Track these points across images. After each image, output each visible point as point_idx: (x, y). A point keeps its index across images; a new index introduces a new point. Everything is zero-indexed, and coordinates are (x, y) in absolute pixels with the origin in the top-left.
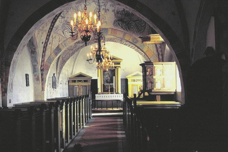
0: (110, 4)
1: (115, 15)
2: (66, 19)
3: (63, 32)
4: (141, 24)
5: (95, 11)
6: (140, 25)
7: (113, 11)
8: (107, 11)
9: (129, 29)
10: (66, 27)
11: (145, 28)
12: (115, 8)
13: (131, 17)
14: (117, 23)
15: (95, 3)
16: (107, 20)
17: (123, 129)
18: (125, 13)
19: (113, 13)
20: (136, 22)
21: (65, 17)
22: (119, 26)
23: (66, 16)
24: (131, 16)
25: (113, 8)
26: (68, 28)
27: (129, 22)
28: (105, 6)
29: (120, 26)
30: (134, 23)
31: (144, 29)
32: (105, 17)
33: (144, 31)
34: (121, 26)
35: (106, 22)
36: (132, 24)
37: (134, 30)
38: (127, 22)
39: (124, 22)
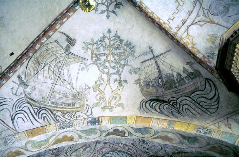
1: (142, 90)
2: (28, 90)
3: (12, 117)
4: (206, 96)
5: (96, 82)
6: (203, 99)
7: (137, 82)
9: (179, 112)
10: (26, 109)
11: (219, 98)
12: (140, 75)
13: (179, 88)
14: (147, 105)
15: (98, 67)
16: (123, 101)
17: (95, 130)
18: (163, 82)
19: (137, 87)
20: (193, 95)
21: (27, 86)
22: (154, 111)
23: (31, 84)
24: (177, 85)
25: (136, 77)
26: (28, 112)
27: (176, 99)
28: (120, 75)
29: (156, 110)
31: (216, 103)
32: (120, 95)
33: (218, 107)
34: (158, 110)
35: (121, 105)
37: (194, 112)
39: (165, 102)
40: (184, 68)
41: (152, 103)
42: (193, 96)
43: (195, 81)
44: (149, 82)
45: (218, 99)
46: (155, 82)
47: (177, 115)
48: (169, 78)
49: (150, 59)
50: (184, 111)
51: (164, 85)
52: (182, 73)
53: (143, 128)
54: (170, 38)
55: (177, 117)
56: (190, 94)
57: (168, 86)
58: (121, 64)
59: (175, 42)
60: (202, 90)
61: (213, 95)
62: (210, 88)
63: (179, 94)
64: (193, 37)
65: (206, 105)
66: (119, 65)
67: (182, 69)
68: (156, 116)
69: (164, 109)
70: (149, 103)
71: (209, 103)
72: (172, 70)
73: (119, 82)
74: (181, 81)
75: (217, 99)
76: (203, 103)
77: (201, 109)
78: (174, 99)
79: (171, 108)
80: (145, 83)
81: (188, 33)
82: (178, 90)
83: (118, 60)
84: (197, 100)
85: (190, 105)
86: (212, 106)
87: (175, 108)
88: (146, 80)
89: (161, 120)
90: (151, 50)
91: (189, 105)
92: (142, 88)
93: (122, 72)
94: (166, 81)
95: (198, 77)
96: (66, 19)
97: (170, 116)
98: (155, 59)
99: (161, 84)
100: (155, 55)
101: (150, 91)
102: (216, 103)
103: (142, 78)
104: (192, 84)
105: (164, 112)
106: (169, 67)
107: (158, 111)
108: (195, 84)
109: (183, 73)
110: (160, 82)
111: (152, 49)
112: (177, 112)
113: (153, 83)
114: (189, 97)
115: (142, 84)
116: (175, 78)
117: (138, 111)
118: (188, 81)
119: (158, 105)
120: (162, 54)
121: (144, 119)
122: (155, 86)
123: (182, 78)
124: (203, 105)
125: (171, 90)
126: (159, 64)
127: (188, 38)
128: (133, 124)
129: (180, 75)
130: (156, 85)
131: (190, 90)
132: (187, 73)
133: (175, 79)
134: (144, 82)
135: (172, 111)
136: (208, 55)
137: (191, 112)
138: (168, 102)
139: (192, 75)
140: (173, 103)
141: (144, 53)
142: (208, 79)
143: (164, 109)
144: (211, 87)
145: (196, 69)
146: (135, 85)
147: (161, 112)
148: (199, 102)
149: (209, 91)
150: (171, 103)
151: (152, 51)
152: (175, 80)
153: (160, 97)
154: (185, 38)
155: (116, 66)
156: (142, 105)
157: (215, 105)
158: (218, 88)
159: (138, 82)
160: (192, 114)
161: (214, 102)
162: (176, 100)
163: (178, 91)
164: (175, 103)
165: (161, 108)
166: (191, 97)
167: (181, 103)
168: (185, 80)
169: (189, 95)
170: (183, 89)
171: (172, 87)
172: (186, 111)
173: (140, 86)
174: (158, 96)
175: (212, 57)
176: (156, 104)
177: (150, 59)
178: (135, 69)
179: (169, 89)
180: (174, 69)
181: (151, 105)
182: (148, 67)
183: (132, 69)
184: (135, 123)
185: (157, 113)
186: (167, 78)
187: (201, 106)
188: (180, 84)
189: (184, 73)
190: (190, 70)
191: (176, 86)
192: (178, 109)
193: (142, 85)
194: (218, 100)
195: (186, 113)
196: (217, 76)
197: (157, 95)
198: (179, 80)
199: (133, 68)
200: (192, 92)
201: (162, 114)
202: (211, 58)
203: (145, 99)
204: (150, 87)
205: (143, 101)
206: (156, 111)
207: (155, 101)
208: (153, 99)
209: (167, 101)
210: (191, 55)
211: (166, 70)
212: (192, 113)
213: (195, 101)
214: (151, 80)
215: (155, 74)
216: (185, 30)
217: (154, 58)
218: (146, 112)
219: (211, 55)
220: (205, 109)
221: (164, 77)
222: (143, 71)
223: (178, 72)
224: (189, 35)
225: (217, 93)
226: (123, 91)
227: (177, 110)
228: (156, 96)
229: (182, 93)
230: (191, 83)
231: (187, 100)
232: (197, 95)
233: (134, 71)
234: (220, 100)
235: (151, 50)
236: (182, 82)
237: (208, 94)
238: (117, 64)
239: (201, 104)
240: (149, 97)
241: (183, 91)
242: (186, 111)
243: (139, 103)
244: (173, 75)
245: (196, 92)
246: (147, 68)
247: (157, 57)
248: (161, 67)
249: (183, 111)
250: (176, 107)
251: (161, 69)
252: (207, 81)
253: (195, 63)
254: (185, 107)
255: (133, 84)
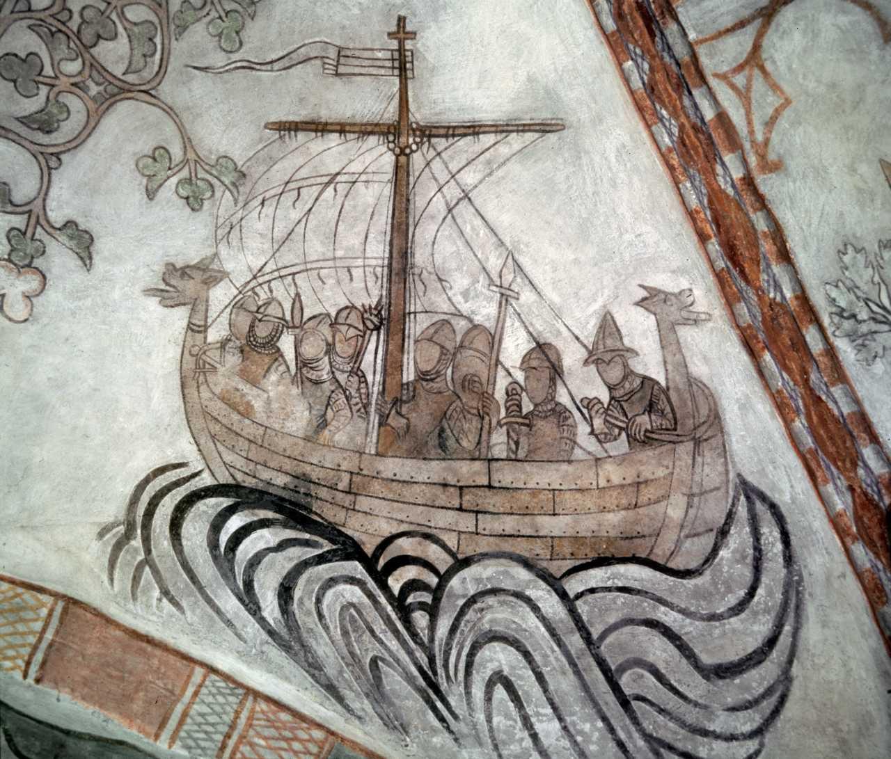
0: (145, 145)
6: (659, 651)
8: (59, 258)
11: (780, 692)
13: (506, 475)
14: (195, 530)
18: (392, 366)
20: (596, 577)
22: (230, 603)
24: (499, 442)
28: (49, 162)
29: (248, 597)
30: (551, 604)
31: (746, 722)
36: (497, 614)
38: (403, 561)
39: (349, 549)
40: (608, 326)
41: (235, 523)
42: (592, 591)
43: (651, 464)
44: (284, 325)
45: (774, 700)
46: (330, 348)
47: (411, 703)
48: (450, 355)
49: (366, 130)
50: (478, 692)
51: (397, 402)
52: (572, 357)
53: (93, 738)
54: (601, 27)
55: (405, 729)
56: (569, 564)
57: (421, 417)
58: (95, 66)
59: (627, 81)
60: (677, 563)
61: (753, 643)
62: (748, 574)
63: (487, 523)
64: (788, 102)
65: (662, 711)
66: (73, 67)
67: (589, 332)
68: (241, 655)
69: (321, 616)
70: (213, 513)
71: (696, 704)
72: (506, 297)
73: (19, 221)
74: (540, 424)
75: (769, 692)
76: (651, 679)
77: (612, 730)
78: (433, 552)
79: (379, 626)
80: (244, 321)
81: (757, 47)
82: (490, 487)
83: (84, 21)
84: (610, 639)
85: (538, 658)
86: (705, 733)
87: (414, 635)
88: (263, 295)
89: (263, 706)
90: (401, 50)
91: (527, 655)
92: (196, 356)
93: (77, 143)
94: (423, 376)
95: (689, 446)
96: (808, 441)
97: (348, 695)
98: (403, 140)
99: (374, 379)
100: (419, 115)
101: (258, 405)
102: (747, 728)
103: (229, 266)
104: (616, 480)
105: (312, 643)
106: (494, 263)
107: (265, 614)
108: (648, 493)
109: (586, 362)
110: (368, 358)
111: (409, 45)
112: (421, 682)
113: (309, 350)
114: (554, 583)
115: (213, 314)
116: (501, 372)
117: (95, 552)
118: (591, 445)
119: (279, 556)
120: (474, 130)
121: (126, 648)
122: (317, 383)
123: (563, 398)
124: (643, 699)
125: (434, 470)
126: (419, 202)
127: (744, 95)
128: (18, 675)
129: (556, 371)
130: (325, 376)
131: (586, 525)
132: (615, 374)
133: (502, 383)
134: (238, 305)
135: (374, 649)
136: (843, 304)
137: (527, 723)
138: (369, 563)
139: (651, 408)
140: (412, 586)
141: (333, 53)
142: (763, 498)
143: (321, 616)
144: (757, 569)
145: (699, 369)
146: (153, 303)
147: (284, 632)
148: (621, 660)
149: (732, 600)
150: (396, 583)
151: (402, 65)
152: (500, 395)
153: (323, 493)
154: (723, 77)
155: (48, 71)
156: (149, 514)
157: (731, 738)
158: (810, 609)
159: (190, 287)
160: (528, 743)
161: (733, 709)
162: (442, 570)
163: (492, 501)
164: (424, 587)
165: (297, 594)
166: (574, 586)
167: (470, 615)
168: (575, 426)
169: (558, 568)
170: (535, 492)
171: (451, 443)
172: (488, 698)
173: (191, 328)
174: (305, 478)
175: (864, 328)
176: (273, 542)
177: (366, 130)
178: (199, 161)
179: (418, 453)
180: (527, 296)
181: (224, 538)
182: (315, 191)
183: (177, 151)
184: (34, 669)
185: (251, 628)
186: (436, 352)
187: (625, 703)
188: (523, 440)
189: (593, 367)
190: (650, 364)
191: (489, 448)
192: (432, 660)
193: (214, 335)
194: (768, 705)
195: (481, 717)
196: (840, 507)
197: (308, 469)
198: (527, 407)
199: (187, 142)
200: (593, 555)
201: (286, 648)
202: (851, 336)
203: (196, 464)
204: (273, 377)
205: (172, 476)
206: (248, 597)
207: (270, 515)
208: (261, 486)
209: (369, 549)
210: (714, 246)
211: (459, 282)
212: (534, 737)
213: (595, 636)
214: (307, 315)
215: (357, 273)
216: (746, 13)
217: (398, 134)
218: (165, 593)
219: (863, 315)
220: (648, 737)
221: (417, 326)
222: (268, 210)
223: (548, 337)
224: (762, 69)
225: (784, 640)
226: (31, 328)
227: (424, 661)
228: (288, 465)
229: (509, 524)
230: (613, 473)
231: (528, 600)
232: (623, 590)
233: (184, 174)
234: (791, 709)
235: (401, 50)
236: (545, 428)
237: (713, 617)
238: (62, 51)
239: (626, 682)
240: (229, 457)
241: (526, 512)
242: (488, 698)
243: (129, 490)
244: (494, 341)
245: (624, 561)
246: (309, 194)
247: (427, 133)
248: (423, 235)
249: (468, 693)
250: (424, 635)
251: (420, 257)
252: (742, 510)
253: (710, 316)
254: (498, 657)
255: (137, 290)
